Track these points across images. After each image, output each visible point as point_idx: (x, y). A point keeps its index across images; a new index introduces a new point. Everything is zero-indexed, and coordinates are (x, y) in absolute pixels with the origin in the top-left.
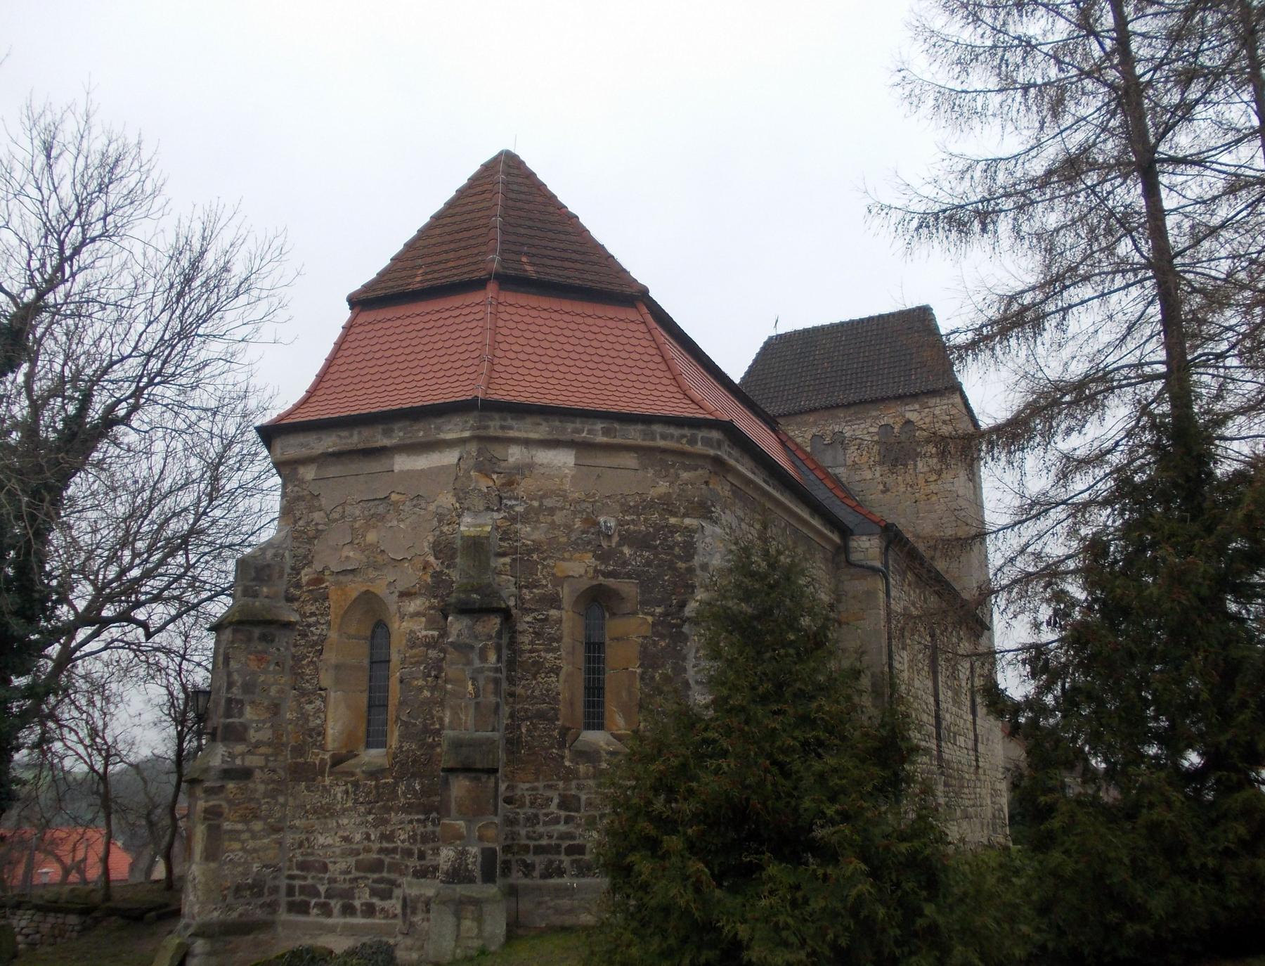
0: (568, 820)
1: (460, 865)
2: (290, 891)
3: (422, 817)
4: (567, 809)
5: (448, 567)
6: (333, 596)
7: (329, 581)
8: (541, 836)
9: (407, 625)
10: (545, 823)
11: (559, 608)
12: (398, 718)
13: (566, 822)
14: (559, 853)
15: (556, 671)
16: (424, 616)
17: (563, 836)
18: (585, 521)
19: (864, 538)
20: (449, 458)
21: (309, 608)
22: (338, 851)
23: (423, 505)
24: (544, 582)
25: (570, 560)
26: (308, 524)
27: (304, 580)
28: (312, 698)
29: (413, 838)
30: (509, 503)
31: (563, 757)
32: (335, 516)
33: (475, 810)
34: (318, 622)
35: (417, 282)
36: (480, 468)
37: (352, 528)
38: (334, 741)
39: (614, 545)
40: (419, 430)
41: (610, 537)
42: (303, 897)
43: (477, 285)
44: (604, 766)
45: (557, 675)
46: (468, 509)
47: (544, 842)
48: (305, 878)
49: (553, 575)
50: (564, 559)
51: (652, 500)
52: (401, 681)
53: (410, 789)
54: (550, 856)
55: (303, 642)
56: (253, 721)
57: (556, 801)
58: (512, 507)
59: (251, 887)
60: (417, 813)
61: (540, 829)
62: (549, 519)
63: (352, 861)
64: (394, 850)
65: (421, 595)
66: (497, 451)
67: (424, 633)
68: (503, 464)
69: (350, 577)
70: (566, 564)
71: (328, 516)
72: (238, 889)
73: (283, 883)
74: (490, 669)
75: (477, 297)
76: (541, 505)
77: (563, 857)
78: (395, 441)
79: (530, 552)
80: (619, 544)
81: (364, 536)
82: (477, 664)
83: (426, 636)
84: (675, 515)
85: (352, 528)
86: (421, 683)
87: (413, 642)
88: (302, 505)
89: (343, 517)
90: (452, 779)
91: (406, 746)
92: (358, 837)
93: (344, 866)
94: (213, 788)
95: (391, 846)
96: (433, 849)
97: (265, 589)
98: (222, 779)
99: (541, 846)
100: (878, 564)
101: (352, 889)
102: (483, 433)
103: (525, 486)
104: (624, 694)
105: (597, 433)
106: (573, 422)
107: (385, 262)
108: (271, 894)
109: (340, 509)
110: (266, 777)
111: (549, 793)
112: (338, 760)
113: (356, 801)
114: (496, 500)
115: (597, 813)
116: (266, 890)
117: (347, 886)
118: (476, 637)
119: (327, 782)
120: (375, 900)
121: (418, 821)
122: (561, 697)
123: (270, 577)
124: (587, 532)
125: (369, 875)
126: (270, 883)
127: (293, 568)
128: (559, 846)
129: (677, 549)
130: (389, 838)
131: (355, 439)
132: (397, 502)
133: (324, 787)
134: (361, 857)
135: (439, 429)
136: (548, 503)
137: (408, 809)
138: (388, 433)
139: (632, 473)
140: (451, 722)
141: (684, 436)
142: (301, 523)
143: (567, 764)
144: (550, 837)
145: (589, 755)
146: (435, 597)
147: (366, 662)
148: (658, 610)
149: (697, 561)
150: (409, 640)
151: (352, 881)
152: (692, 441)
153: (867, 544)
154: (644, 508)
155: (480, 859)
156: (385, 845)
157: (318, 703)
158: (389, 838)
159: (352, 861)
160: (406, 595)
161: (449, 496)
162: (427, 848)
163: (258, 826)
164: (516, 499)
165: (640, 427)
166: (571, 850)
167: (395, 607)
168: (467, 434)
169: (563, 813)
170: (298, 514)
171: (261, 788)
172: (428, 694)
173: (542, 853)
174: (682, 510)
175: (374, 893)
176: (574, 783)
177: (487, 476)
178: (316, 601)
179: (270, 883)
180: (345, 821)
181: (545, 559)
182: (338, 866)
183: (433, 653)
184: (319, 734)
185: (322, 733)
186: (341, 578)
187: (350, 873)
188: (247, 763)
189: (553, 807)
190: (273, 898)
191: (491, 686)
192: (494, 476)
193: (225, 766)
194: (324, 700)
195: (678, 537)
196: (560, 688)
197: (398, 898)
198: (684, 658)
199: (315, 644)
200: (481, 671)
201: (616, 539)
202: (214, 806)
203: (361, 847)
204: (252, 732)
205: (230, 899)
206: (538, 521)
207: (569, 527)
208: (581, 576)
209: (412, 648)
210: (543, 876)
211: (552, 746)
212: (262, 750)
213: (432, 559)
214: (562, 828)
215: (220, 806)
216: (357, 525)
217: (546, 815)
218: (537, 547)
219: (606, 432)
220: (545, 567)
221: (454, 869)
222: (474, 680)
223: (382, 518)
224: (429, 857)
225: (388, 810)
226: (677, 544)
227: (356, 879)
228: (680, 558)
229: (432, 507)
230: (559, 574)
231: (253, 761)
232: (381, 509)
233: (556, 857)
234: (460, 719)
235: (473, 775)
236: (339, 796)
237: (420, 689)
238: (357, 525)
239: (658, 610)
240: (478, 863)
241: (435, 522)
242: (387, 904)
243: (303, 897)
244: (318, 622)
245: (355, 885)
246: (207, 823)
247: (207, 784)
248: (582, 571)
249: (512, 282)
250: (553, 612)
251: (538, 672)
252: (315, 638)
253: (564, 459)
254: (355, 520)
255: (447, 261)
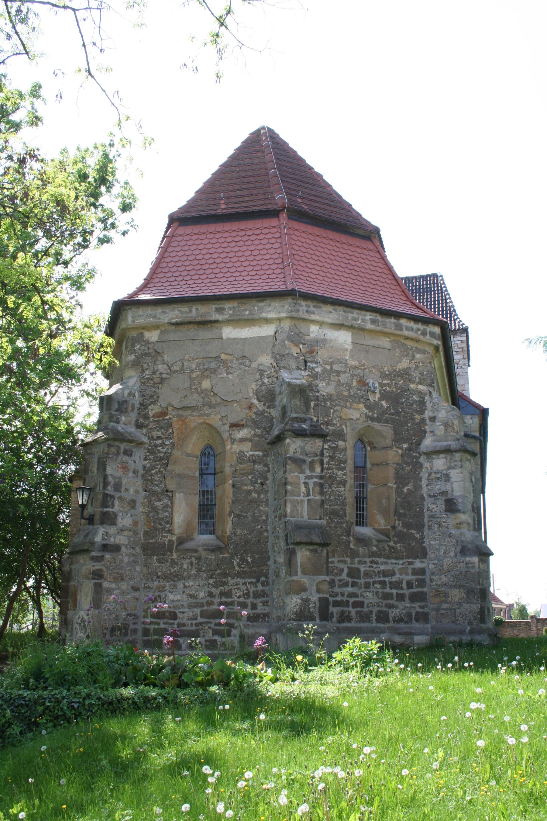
0: (354, 584)
1: (305, 608)
2: (146, 632)
3: (254, 580)
4: (352, 577)
5: (269, 407)
6: (176, 426)
7: (171, 413)
8: (337, 595)
9: (236, 448)
10: (340, 586)
11: (344, 441)
12: (231, 512)
13: (352, 586)
14: (348, 606)
15: (343, 483)
16: (250, 440)
17: (351, 595)
18: (359, 382)
19: (468, 417)
20: (268, 331)
21: (155, 434)
22: (185, 604)
23: (248, 363)
24: (335, 422)
25: (350, 408)
26: (154, 373)
27: (151, 414)
28: (161, 497)
29: (247, 595)
30: (311, 365)
31: (349, 542)
32: (175, 368)
33: (313, 570)
34: (163, 444)
35: (223, 208)
36: (291, 339)
37: (191, 378)
38: (179, 527)
39: (377, 400)
40: (245, 310)
41: (374, 392)
42: (156, 637)
43: (273, 213)
44: (375, 549)
45: (345, 486)
46: (284, 367)
47: (339, 598)
48: (158, 624)
49: (341, 417)
50: (346, 407)
51: (400, 371)
52: (234, 486)
53: (243, 560)
54: (342, 608)
55: (152, 458)
56: (120, 511)
57: (346, 571)
58: (313, 368)
59: (120, 629)
60: (249, 578)
61: (337, 590)
62: (337, 379)
63: (198, 611)
64: (232, 603)
65: (247, 426)
66: (302, 327)
67: (251, 453)
68: (307, 338)
69: (189, 412)
70: (349, 411)
71: (169, 368)
72: (113, 630)
73: (140, 627)
74: (316, 477)
75: (274, 222)
76: (332, 368)
77: (351, 609)
78: (226, 317)
79: (325, 400)
80: (380, 399)
81: (200, 384)
82: (308, 473)
83: (252, 455)
84: (413, 382)
85: (191, 378)
86: (249, 488)
87: (241, 458)
88: (148, 359)
89: (182, 369)
90: (297, 548)
91: (239, 532)
92: (202, 595)
93: (191, 615)
94: (97, 557)
95: (229, 600)
96: (263, 603)
97: (123, 418)
98: (103, 551)
99: (337, 601)
100: (477, 434)
101: (198, 630)
102: (294, 314)
103: (322, 354)
104: (384, 501)
105: (366, 319)
106: (353, 313)
107: (191, 194)
108: (132, 634)
109: (179, 363)
110: (128, 552)
111: (341, 566)
112: (181, 541)
113: (199, 570)
114: (303, 363)
115: (371, 580)
116: (129, 632)
117: (194, 628)
118: (307, 454)
119: (175, 556)
120: (216, 637)
121: (251, 583)
122: (347, 501)
123: (126, 409)
124: (360, 390)
125: (211, 620)
126: (132, 627)
127: (141, 404)
128: (348, 602)
129: (415, 406)
130: (228, 594)
131: (196, 312)
132: (226, 360)
133: (173, 560)
134: (205, 608)
135: (261, 310)
136: (336, 367)
137: (239, 575)
138: (220, 310)
139: (387, 351)
140: (291, 512)
141: (419, 329)
142: (147, 372)
143: (352, 546)
144: (343, 595)
145: (362, 541)
146: (259, 428)
147: (197, 474)
148: (405, 446)
149: (428, 414)
150: (238, 458)
151: (197, 625)
152: (424, 333)
153: (471, 421)
154: (395, 376)
155: (318, 604)
156: (224, 599)
157: (166, 501)
158: (228, 594)
159: (198, 611)
160: (236, 426)
161: (269, 357)
162: (258, 602)
163: (124, 586)
164: (317, 363)
165: (393, 320)
166: (356, 605)
167: (227, 434)
168: (284, 315)
169: (350, 580)
170: (145, 366)
171: (126, 559)
172: (256, 496)
173: (338, 606)
174: (417, 380)
175: (215, 632)
176: (356, 560)
177: (297, 345)
178: (162, 428)
179: (132, 627)
180: (191, 583)
181: (335, 406)
182: (186, 614)
183: (258, 467)
184: (167, 523)
185: (170, 521)
186: (181, 412)
187: (196, 619)
188: (117, 542)
189: (344, 575)
190: (133, 637)
191: (318, 489)
192: (301, 346)
193: (104, 542)
194: (171, 498)
195: (415, 398)
196: (347, 495)
197: (235, 636)
198: (421, 480)
199: (162, 459)
200: (310, 477)
201: (378, 396)
202: (98, 570)
203: (204, 601)
204: (119, 519)
205: (108, 637)
206: (329, 379)
207: (349, 386)
208: (358, 419)
209: (241, 463)
210: (339, 622)
211: (342, 535)
212: (126, 533)
213: (255, 401)
214: (350, 589)
215: (101, 570)
216: (194, 376)
217: (340, 580)
218: (330, 397)
219: (373, 322)
220: (335, 411)
221: (301, 611)
222: (306, 484)
223: (214, 371)
224: (259, 608)
225: (226, 575)
226: (415, 402)
227: (201, 624)
228: (417, 412)
229: (254, 365)
230: (344, 417)
231: (121, 540)
232: (213, 365)
233: (345, 609)
234: (297, 510)
235: (311, 547)
236: (185, 566)
237: (249, 492)
238: (194, 376)
239: (405, 446)
240: (317, 608)
241: (258, 376)
242: (227, 640)
243: (156, 637)
244: (163, 444)
245: (200, 627)
246: (94, 581)
247: (93, 554)
248: (358, 416)
249: (298, 215)
250: (341, 443)
251: (332, 484)
252: (162, 455)
253: (344, 338)
254: (192, 371)
255: (242, 196)
